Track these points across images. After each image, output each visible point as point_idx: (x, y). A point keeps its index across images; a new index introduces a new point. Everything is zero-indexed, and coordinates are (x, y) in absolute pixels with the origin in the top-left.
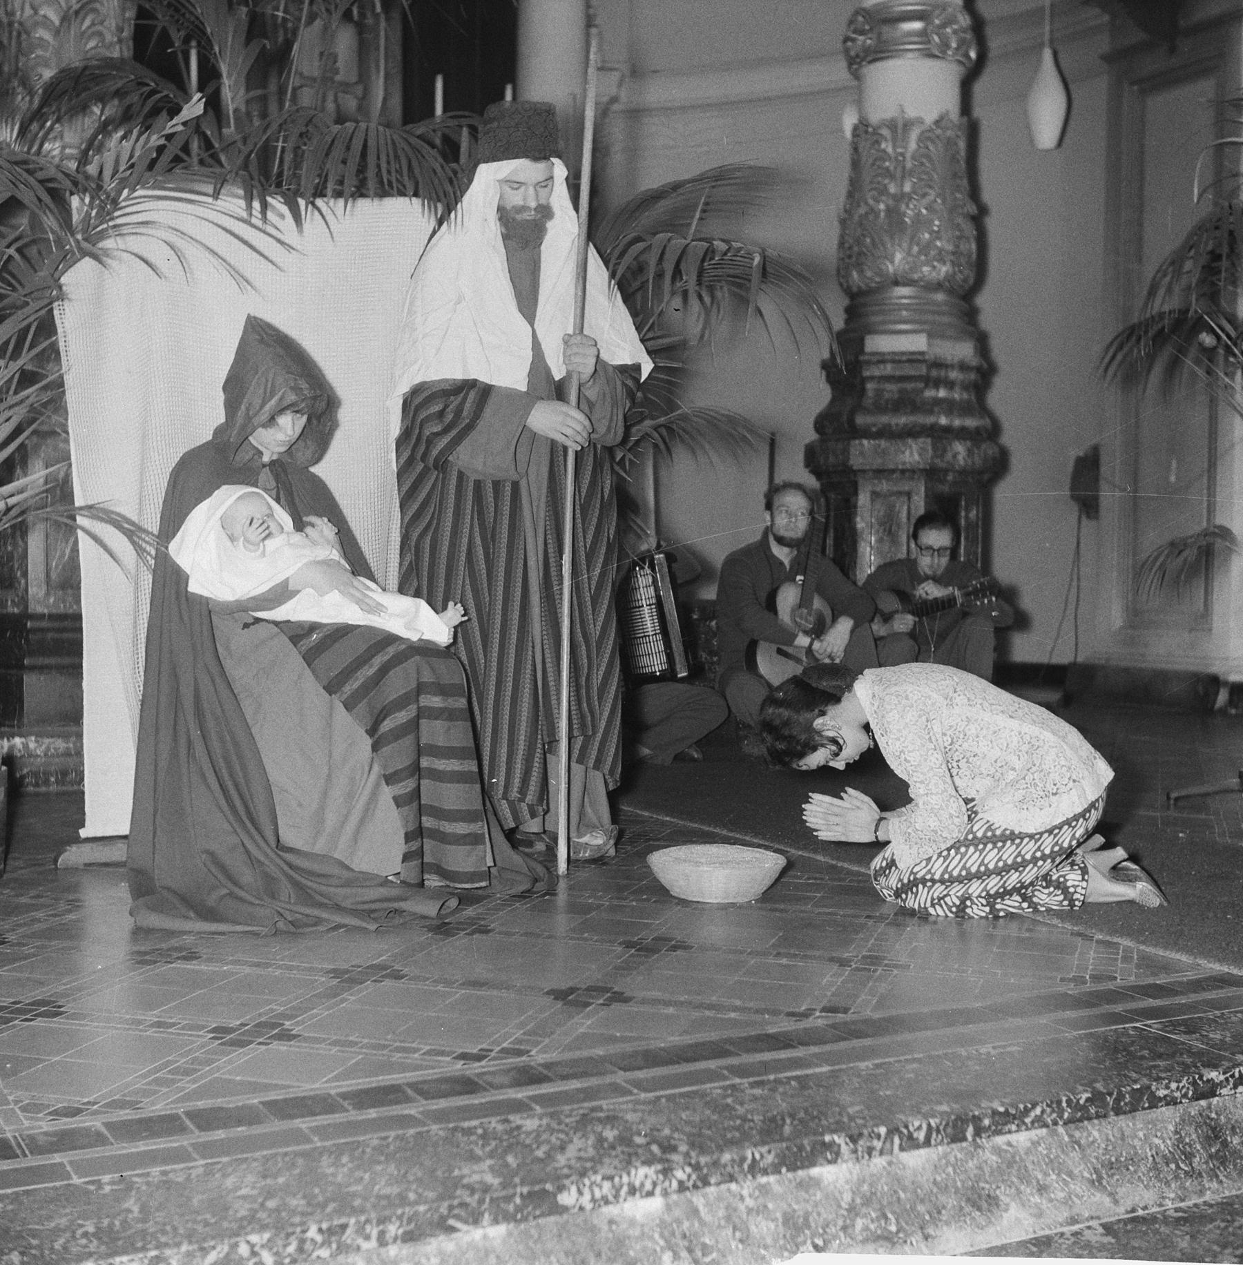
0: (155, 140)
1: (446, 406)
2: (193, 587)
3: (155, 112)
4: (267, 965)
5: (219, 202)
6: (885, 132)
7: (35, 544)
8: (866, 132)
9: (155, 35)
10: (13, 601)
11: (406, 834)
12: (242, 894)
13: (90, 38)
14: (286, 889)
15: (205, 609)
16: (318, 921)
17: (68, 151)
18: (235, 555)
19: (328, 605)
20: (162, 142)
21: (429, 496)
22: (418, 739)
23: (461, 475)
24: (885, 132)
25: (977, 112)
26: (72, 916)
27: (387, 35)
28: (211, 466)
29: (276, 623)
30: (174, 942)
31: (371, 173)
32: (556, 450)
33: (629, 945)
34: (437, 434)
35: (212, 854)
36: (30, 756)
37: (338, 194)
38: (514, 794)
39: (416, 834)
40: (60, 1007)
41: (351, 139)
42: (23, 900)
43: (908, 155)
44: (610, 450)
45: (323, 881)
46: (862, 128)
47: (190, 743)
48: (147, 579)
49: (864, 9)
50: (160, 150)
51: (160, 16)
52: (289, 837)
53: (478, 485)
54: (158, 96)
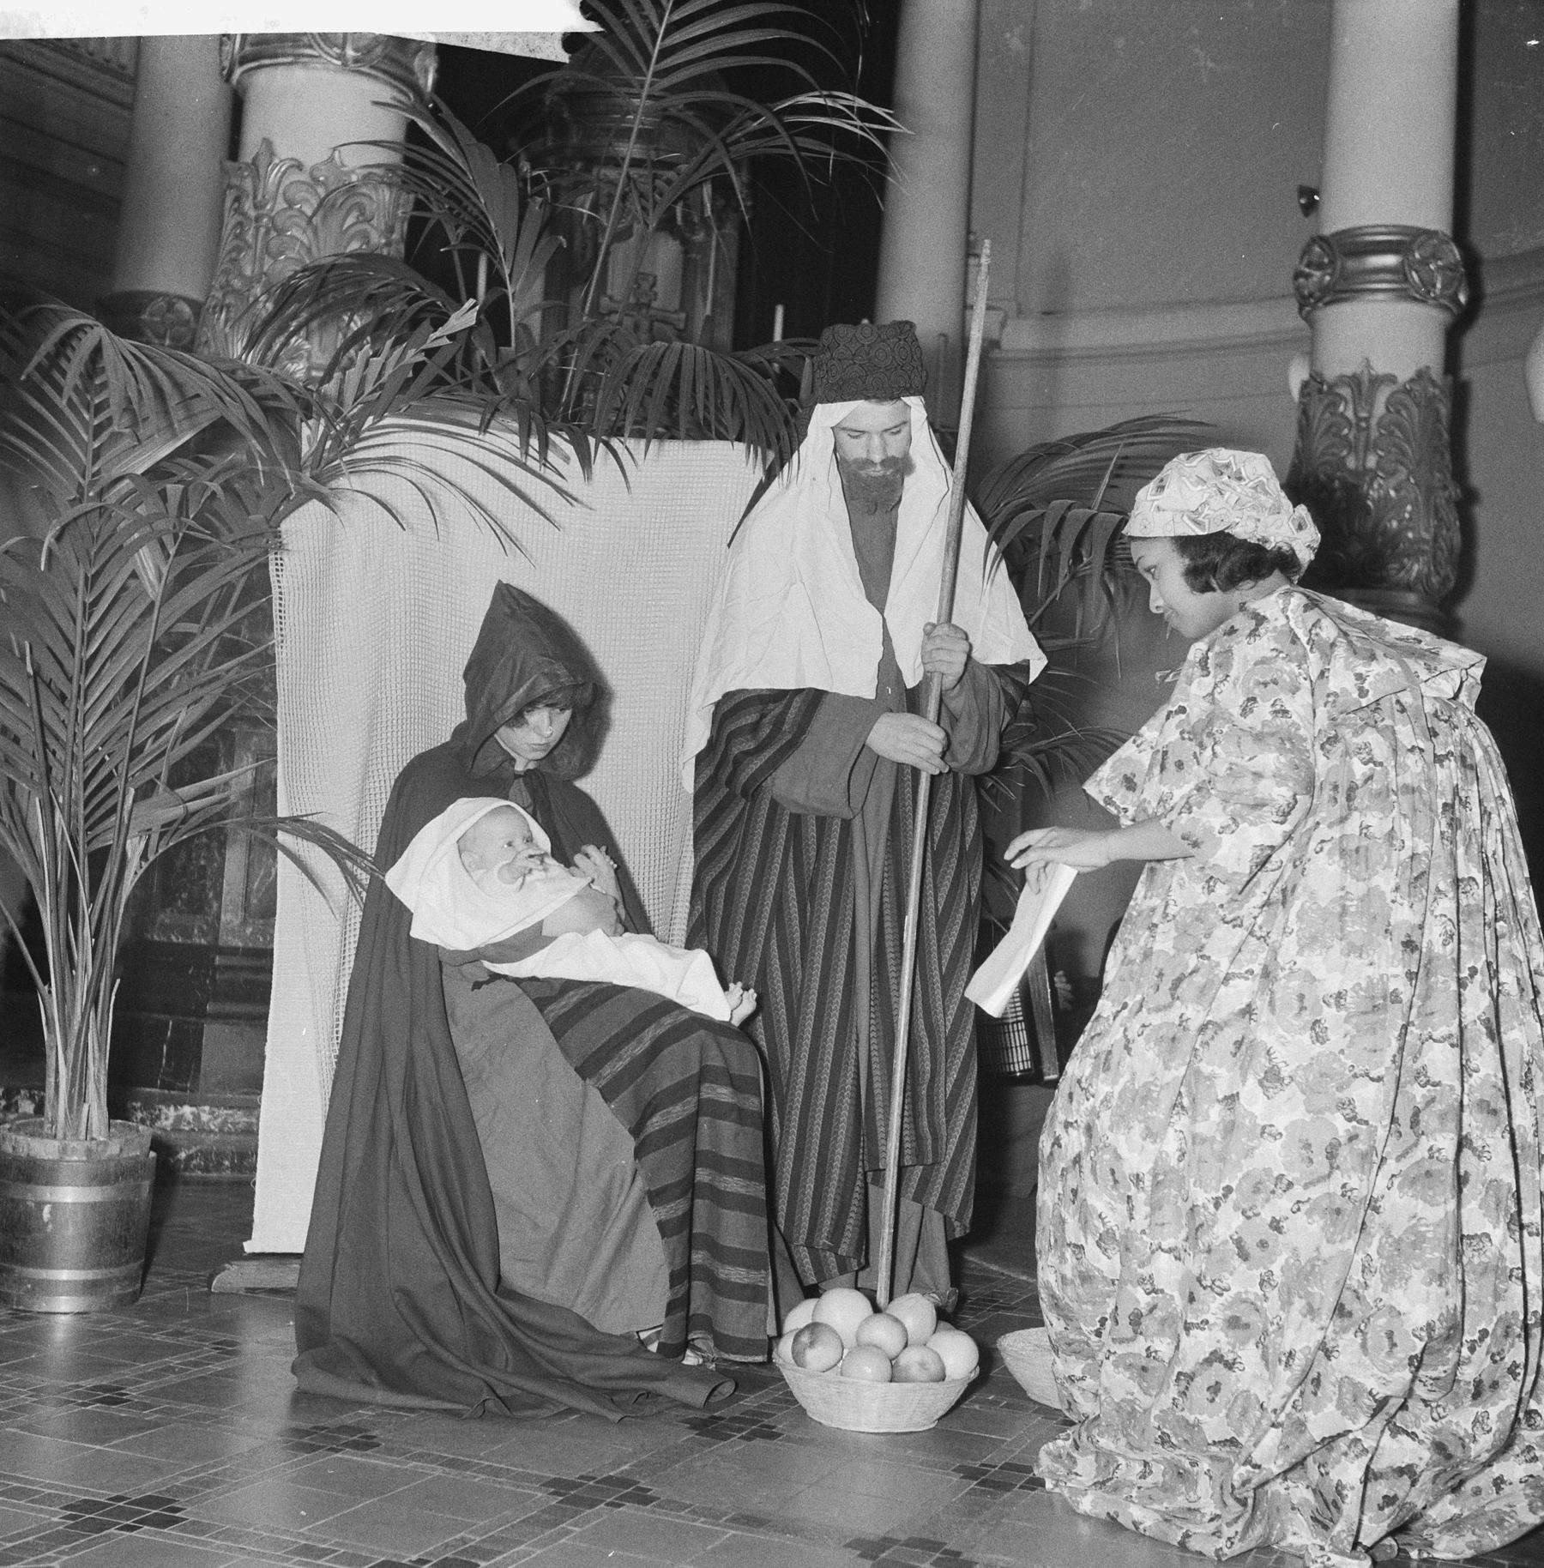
0: (413, 356)
1: (763, 716)
2: (416, 932)
3: (415, 323)
4: (466, 1466)
5: (488, 437)
6: (1345, 391)
7: (234, 861)
8: (1320, 391)
9: (427, 230)
10: (201, 929)
11: (671, 1275)
12: (445, 1355)
13: (352, 238)
14: (503, 1353)
15: (435, 960)
16: (541, 1402)
17: (314, 373)
18: (472, 886)
19: (595, 956)
20: (421, 358)
21: (733, 828)
22: (695, 1143)
23: (774, 805)
24: (1345, 391)
25: (1467, 373)
26: (216, 1367)
27: (718, 246)
28: (447, 773)
29: (518, 981)
30: (348, 1419)
31: (683, 405)
32: (906, 775)
33: (970, 1474)
34: (748, 754)
35: (406, 1293)
36: (202, 1130)
37: (639, 434)
38: (823, 1240)
39: (682, 1275)
40: (178, 1510)
41: (659, 364)
42: (159, 1337)
43: (1374, 422)
44: (978, 780)
45: (551, 1342)
46: (1315, 385)
47: (392, 1141)
48: (357, 915)
49: (1323, 239)
50: (418, 368)
51: (435, 209)
52: (517, 1274)
53: (797, 821)
54: (422, 303)
